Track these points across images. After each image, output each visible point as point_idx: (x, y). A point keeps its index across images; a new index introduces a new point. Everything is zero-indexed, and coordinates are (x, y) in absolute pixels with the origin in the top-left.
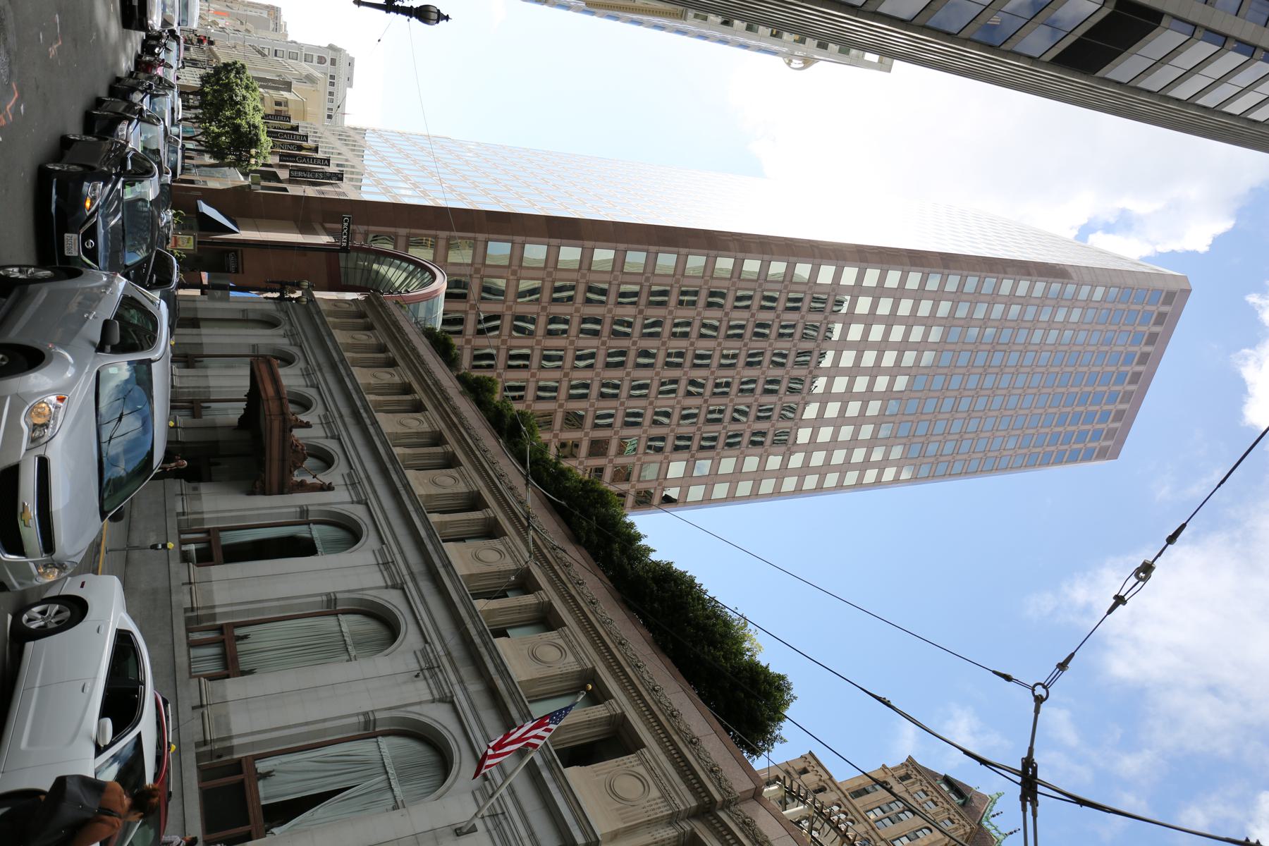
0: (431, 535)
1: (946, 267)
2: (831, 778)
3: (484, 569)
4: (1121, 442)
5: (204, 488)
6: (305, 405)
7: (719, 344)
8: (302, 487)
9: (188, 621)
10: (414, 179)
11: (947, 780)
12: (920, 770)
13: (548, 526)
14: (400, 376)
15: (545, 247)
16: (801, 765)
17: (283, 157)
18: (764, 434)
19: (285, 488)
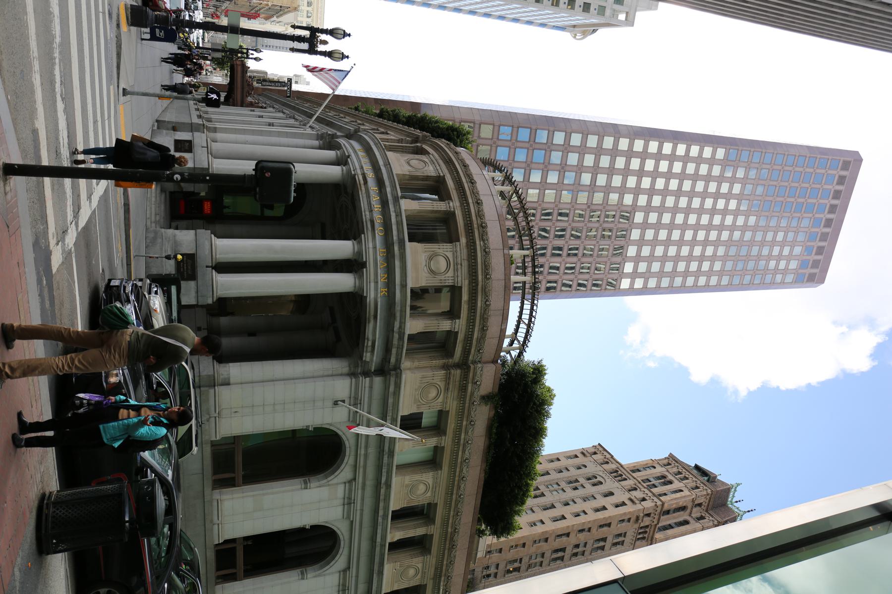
2: (612, 457)
4: (825, 271)
11: (697, 467)
12: (676, 461)
16: (593, 450)
18: (560, 249)
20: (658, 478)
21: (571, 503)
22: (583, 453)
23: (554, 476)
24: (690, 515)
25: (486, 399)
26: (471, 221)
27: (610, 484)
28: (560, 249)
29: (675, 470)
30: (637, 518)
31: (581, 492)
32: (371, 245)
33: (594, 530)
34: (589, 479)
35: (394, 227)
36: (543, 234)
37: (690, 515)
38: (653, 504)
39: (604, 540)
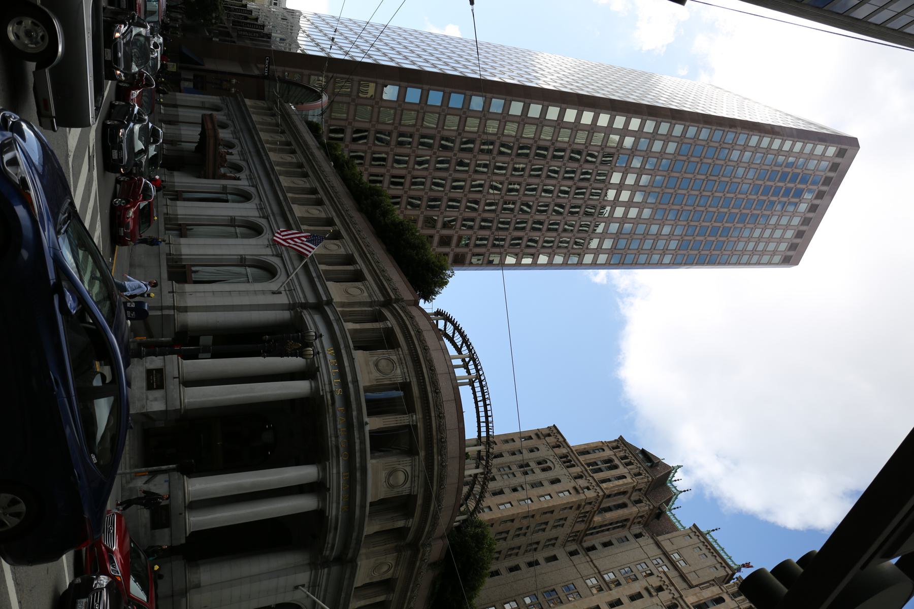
0: (319, 277)
1: (674, 118)
2: (565, 440)
3: (328, 252)
5: (175, 173)
6: (230, 146)
7: (512, 160)
8: (224, 177)
9: (165, 219)
10: (308, 33)
11: (643, 452)
13: (348, 203)
14: (326, 212)
15: (397, 88)
16: (548, 432)
17: (234, 23)
18: (541, 223)
19: (215, 176)
20: (606, 462)
21: (519, 489)
22: (537, 435)
23: (507, 458)
24: (629, 498)
25: (433, 565)
26: (431, 434)
27: (559, 471)
28: (541, 223)
29: (622, 454)
30: (579, 506)
31: (530, 478)
32: (335, 471)
33: (537, 517)
34: (539, 463)
35: (358, 455)
36: (525, 208)
37: (629, 498)
38: (595, 494)
39: (546, 523)
